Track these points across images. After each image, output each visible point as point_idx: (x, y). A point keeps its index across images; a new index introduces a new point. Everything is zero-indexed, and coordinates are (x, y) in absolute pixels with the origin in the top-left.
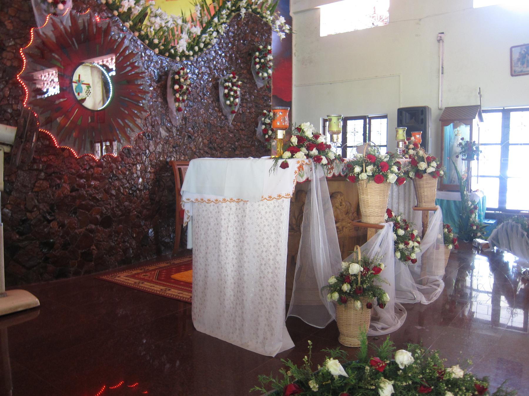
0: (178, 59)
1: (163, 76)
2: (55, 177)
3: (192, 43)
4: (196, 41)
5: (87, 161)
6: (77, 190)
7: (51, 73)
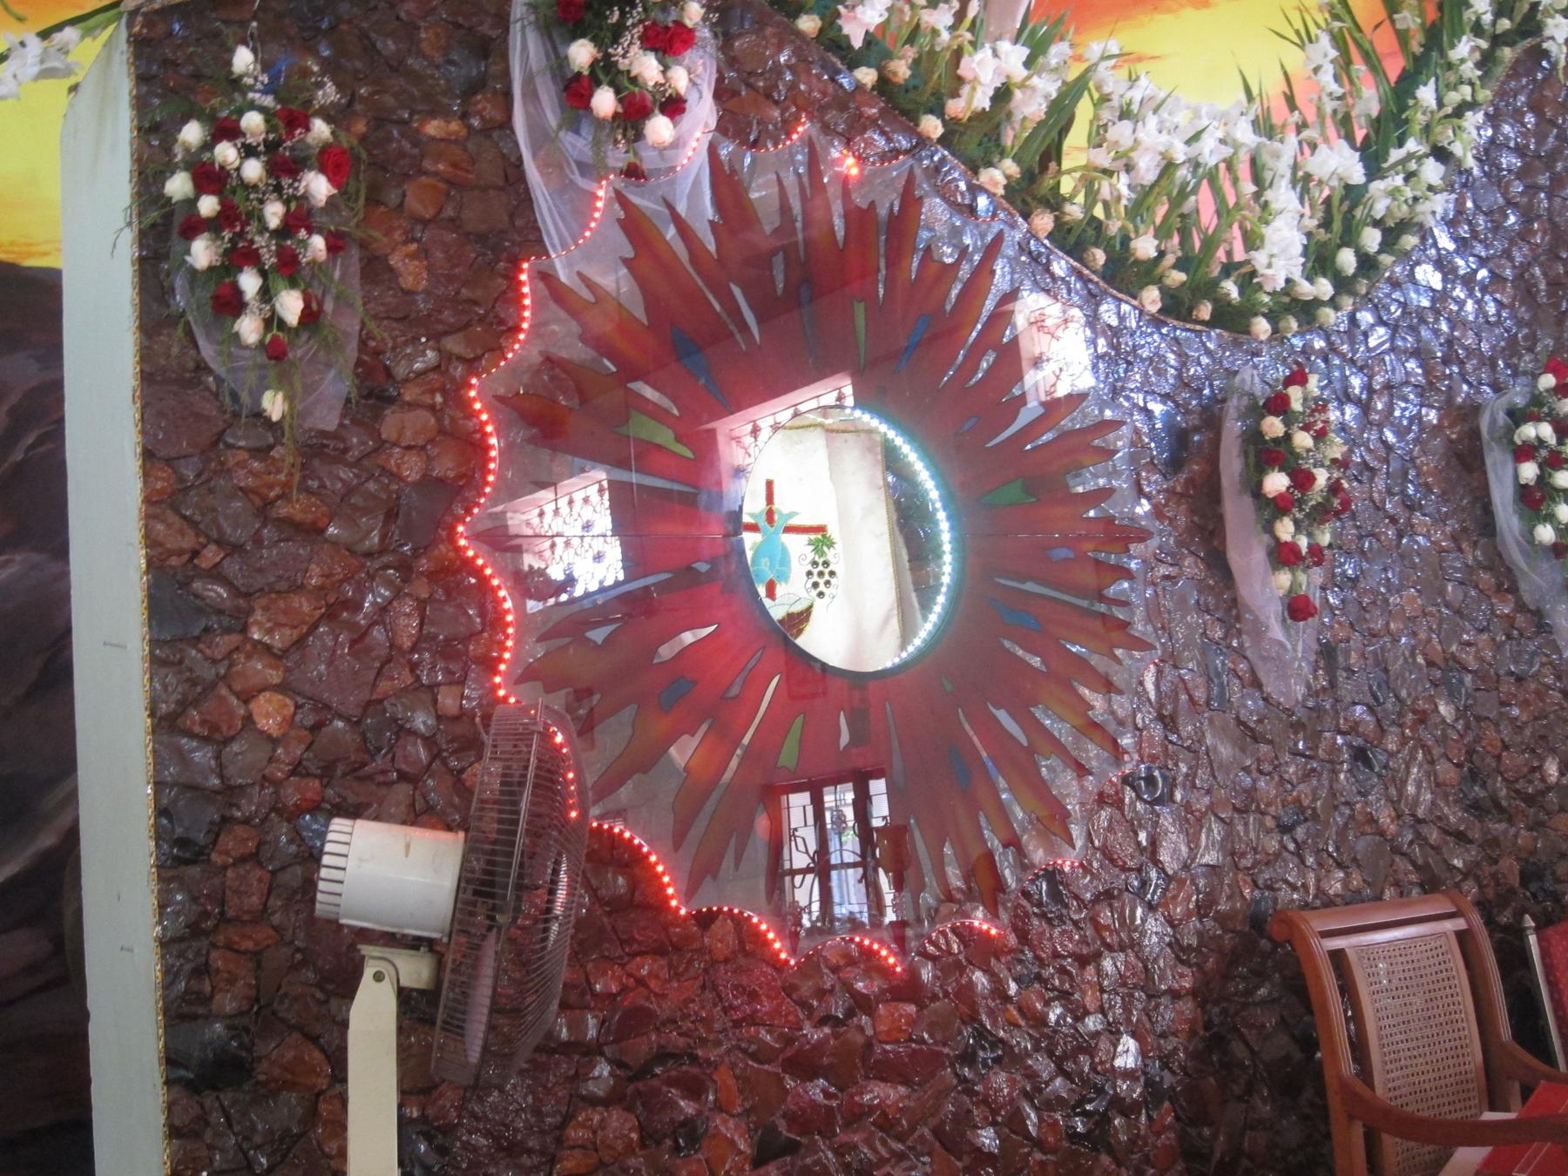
0: (1262, 327)
1: (1196, 430)
2: (671, 1082)
3: (1322, 235)
4: (1337, 225)
5: (835, 970)
6: (792, 1148)
7: (578, 497)
